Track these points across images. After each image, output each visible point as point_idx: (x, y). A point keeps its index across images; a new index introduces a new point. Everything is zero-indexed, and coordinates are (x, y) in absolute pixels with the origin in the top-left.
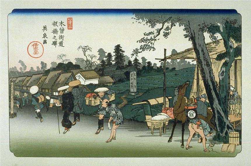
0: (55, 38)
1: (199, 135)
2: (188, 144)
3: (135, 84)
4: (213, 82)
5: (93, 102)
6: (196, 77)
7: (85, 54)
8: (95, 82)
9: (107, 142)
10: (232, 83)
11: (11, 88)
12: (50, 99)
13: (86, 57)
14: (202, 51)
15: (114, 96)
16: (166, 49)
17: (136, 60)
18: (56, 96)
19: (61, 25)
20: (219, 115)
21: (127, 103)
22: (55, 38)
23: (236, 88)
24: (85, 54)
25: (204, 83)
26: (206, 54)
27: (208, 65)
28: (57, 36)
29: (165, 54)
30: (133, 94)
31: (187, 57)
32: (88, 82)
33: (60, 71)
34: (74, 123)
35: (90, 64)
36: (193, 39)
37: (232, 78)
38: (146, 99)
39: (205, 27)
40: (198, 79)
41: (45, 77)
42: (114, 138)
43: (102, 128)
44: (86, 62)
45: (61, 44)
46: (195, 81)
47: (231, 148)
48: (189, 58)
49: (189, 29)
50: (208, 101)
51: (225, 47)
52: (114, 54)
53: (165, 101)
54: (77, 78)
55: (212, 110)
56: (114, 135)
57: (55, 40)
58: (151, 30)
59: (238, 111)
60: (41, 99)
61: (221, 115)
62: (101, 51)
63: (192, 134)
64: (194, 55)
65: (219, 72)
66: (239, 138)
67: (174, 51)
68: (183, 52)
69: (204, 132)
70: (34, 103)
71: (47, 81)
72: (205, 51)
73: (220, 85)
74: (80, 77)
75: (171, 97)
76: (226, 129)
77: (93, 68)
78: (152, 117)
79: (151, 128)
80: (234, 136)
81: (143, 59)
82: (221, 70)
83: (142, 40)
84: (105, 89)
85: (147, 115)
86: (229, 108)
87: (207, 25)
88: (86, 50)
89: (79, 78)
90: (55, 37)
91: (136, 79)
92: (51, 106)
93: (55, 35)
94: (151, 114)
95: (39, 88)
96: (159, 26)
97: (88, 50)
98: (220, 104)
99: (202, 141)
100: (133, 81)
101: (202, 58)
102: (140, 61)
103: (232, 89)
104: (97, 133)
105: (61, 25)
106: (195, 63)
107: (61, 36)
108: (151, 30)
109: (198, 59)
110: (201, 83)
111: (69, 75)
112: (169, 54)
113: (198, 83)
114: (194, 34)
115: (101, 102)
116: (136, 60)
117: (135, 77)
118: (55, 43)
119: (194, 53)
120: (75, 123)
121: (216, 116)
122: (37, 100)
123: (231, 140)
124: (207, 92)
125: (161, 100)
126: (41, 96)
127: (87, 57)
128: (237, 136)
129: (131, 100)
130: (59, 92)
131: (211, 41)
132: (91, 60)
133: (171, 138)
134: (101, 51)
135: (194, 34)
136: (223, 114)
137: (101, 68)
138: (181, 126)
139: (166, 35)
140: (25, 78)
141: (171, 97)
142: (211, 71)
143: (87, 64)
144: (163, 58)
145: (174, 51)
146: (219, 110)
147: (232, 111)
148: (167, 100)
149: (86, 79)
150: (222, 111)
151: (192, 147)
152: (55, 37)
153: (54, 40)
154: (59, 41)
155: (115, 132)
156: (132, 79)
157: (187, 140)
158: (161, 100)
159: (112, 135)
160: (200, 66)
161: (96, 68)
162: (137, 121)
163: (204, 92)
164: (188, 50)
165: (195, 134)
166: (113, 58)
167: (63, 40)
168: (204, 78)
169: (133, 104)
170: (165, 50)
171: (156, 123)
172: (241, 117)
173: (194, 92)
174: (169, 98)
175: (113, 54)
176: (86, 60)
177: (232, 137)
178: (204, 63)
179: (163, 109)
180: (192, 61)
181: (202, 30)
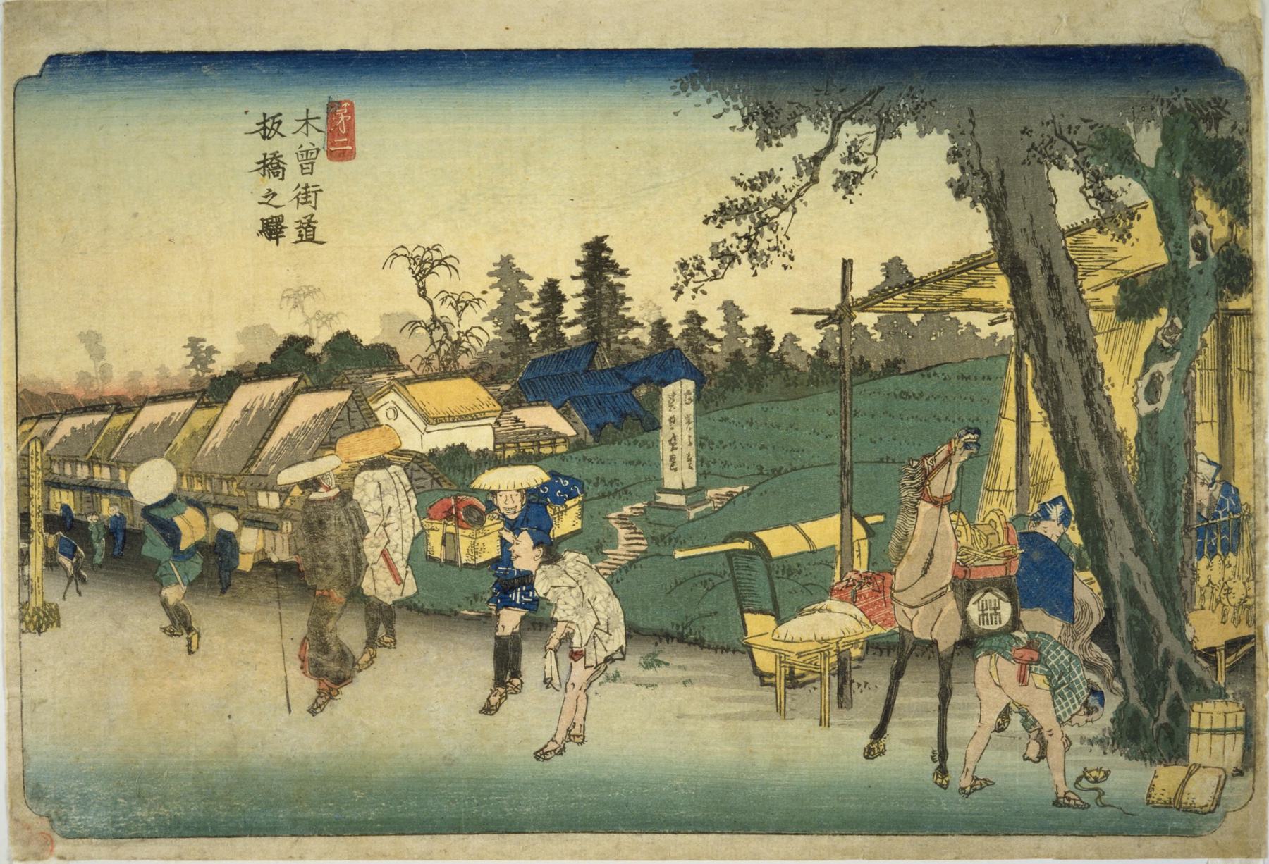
0: (274, 202)
1: (1029, 722)
2: (971, 768)
3: (686, 434)
4: (1107, 438)
5: (464, 544)
6: (1011, 411)
7: (422, 292)
8: (479, 438)
9: (541, 755)
10: (1206, 441)
11: (28, 468)
12: (240, 529)
13: (430, 303)
14: (1048, 265)
15: (576, 510)
16: (851, 261)
17: (695, 319)
18: (267, 511)
19: (304, 129)
20: (1138, 613)
21: (644, 548)
22: (274, 201)
23: (1224, 467)
24: (422, 292)
25: (1056, 441)
26: (1066, 281)
27: (1078, 342)
28: (286, 189)
29: (846, 287)
30: (679, 500)
31: (964, 300)
32: (440, 439)
33: (288, 383)
34: (367, 657)
35: (450, 339)
36: (995, 204)
37: (1205, 410)
38: (748, 529)
39: (1055, 138)
40: (1022, 408)
41: (208, 414)
42: (575, 736)
43: (516, 682)
44: (431, 332)
45: (308, 231)
46: (1009, 430)
47: (1201, 791)
48: (970, 307)
49: (974, 150)
50: (1075, 537)
51: (1167, 247)
52: (581, 286)
53: (846, 539)
54: (381, 415)
55: (1082, 530)
56: (579, 721)
57: (276, 212)
58: (757, 161)
59: (1238, 590)
60: (191, 526)
61: (1144, 609)
62: (507, 272)
63: (991, 718)
64: (999, 290)
65: (1136, 381)
66: (1240, 738)
67: (894, 268)
68: (946, 275)
69: (1055, 706)
70: (154, 547)
71: (217, 438)
72: (1061, 269)
73: (1140, 450)
74: (396, 409)
75: (881, 518)
76: (1175, 687)
77: (465, 361)
78: (780, 622)
79: (773, 680)
80: (1219, 725)
81: (731, 311)
82: (1145, 368)
83: (724, 213)
84: (533, 476)
85: (750, 611)
86: (1189, 573)
87: (1070, 127)
88: (427, 266)
89: (391, 414)
90: (275, 194)
91: (692, 419)
92: (245, 563)
93: (273, 183)
94: (769, 606)
95: (180, 475)
96: (809, 137)
97: (441, 270)
98: (1139, 551)
99: (1042, 755)
100: (678, 434)
101: (1041, 301)
102: (715, 324)
103: (1206, 471)
104: (488, 710)
105: (304, 129)
106: (1007, 329)
107: (307, 187)
108: (757, 161)
109: (1023, 312)
110: (1041, 436)
111: (335, 398)
112: (866, 280)
113: (1022, 439)
114: (1001, 181)
115: (504, 544)
116: (695, 319)
117: (690, 409)
118: (272, 230)
119: (1002, 283)
120: (372, 658)
121: (1122, 617)
122: (171, 533)
123: (1199, 749)
124: (1069, 488)
125: (825, 532)
126: (191, 513)
127: (436, 303)
128: (1231, 725)
129: (666, 530)
130: (285, 492)
131: (1091, 215)
132: (454, 319)
133: (879, 733)
134: (507, 272)
135: (1001, 181)
136: (1149, 597)
137: (508, 361)
138: (934, 674)
139: (848, 182)
140: (98, 418)
141: (881, 518)
142: (1091, 379)
143: (433, 343)
144: (832, 300)
145: (894, 268)
146: (1140, 588)
147: (1209, 589)
148: (859, 531)
149: (427, 422)
150: (1150, 588)
151: (987, 782)
152: (275, 194)
153: (268, 212)
154: (292, 216)
155: (582, 705)
156: (672, 420)
157: (965, 743)
158: (825, 532)
159: (565, 723)
160: (1032, 349)
161: (483, 365)
162: (700, 643)
163: (1058, 485)
164: (970, 267)
165: (1006, 713)
166: (571, 310)
167: (315, 208)
168: (1053, 408)
169: (679, 554)
170: (847, 265)
171: (799, 655)
172: (1252, 621)
173: (1003, 488)
174: (870, 520)
175: (572, 288)
176: (426, 316)
177: (1208, 727)
178: (1055, 333)
179: (837, 579)
180: (992, 323)
181: (1038, 156)
